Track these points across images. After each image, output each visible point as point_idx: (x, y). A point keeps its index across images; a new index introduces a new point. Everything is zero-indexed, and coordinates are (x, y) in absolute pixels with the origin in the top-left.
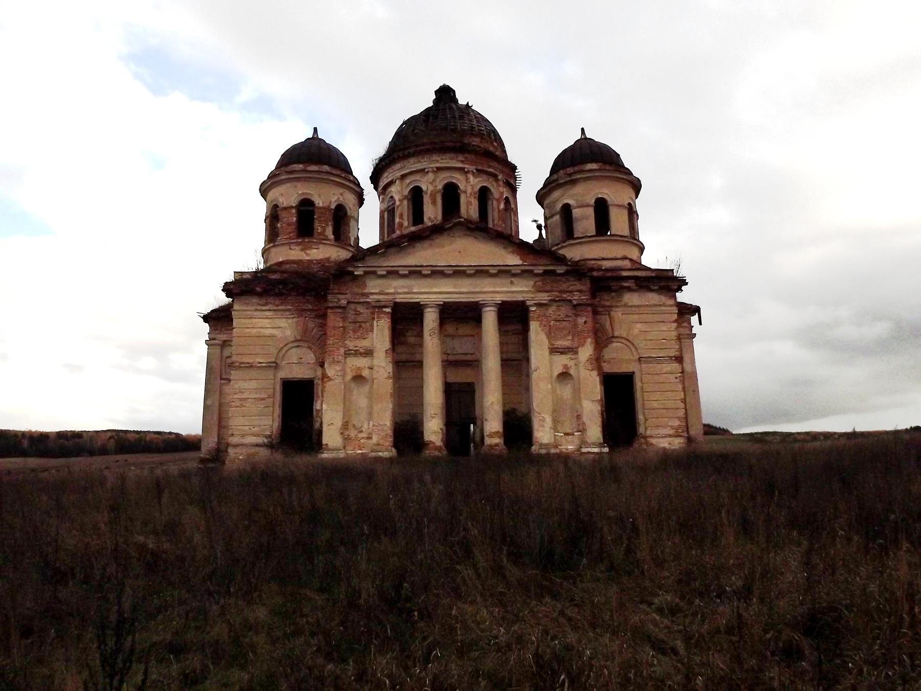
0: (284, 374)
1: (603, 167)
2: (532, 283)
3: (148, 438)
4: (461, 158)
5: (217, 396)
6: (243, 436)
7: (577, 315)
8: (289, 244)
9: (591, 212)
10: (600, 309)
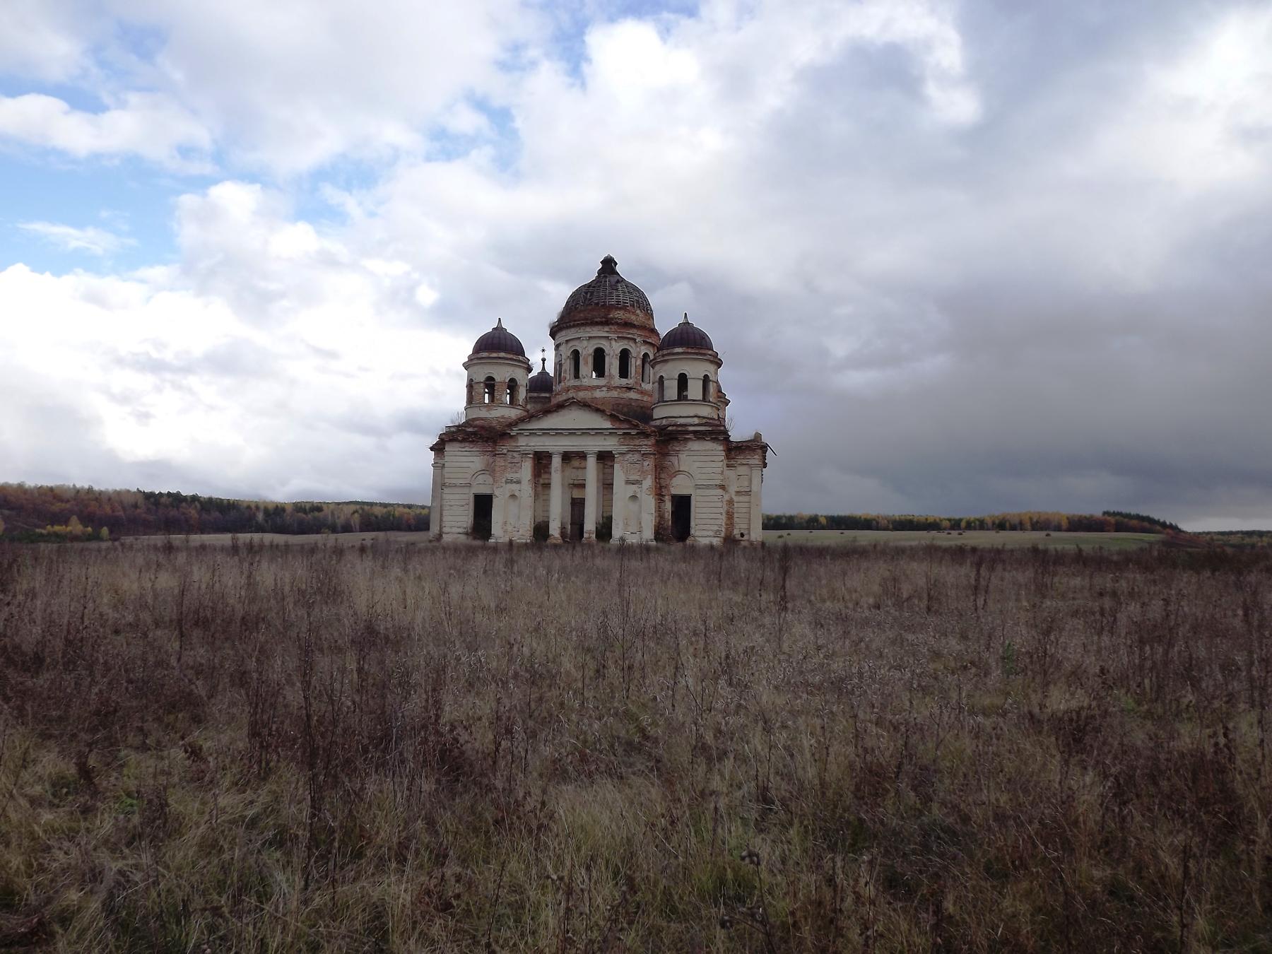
3: (397, 514)
4: (607, 329)
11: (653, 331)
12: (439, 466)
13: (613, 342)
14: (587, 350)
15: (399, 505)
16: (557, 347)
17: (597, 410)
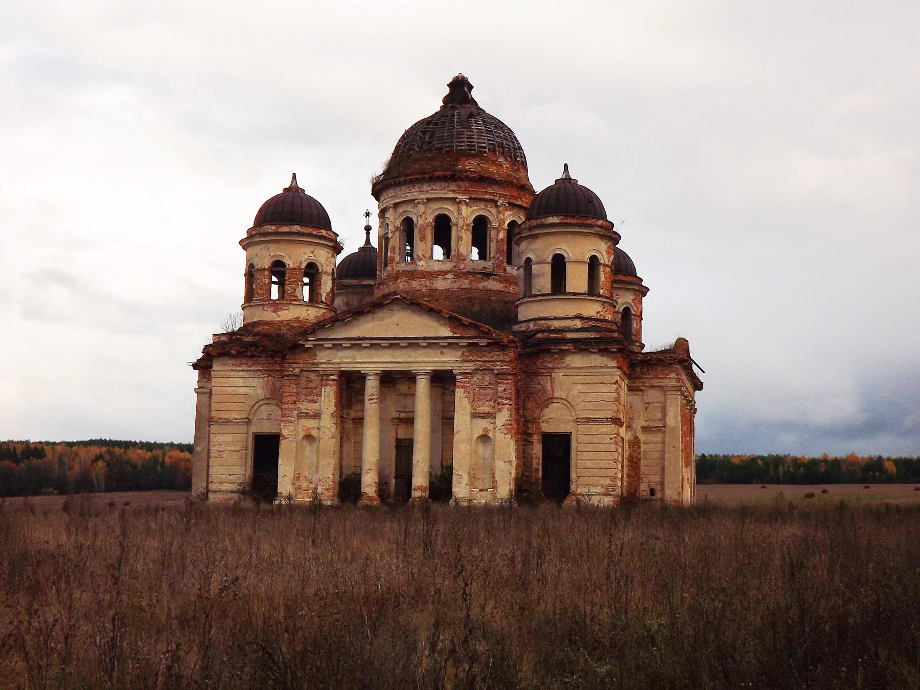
0: (255, 429)
1: (565, 221)
2: (460, 353)
5: (205, 443)
6: (221, 483)
7: (498, 384)
8: (262, 305)
9: (548, 269)
10: (542, 371)
11: (526, 188)
12: (204, 392)
13: (464, 208)
14: (424, 217)
15: (172, 445)
16: (382, 213)
17: (431, 311)
